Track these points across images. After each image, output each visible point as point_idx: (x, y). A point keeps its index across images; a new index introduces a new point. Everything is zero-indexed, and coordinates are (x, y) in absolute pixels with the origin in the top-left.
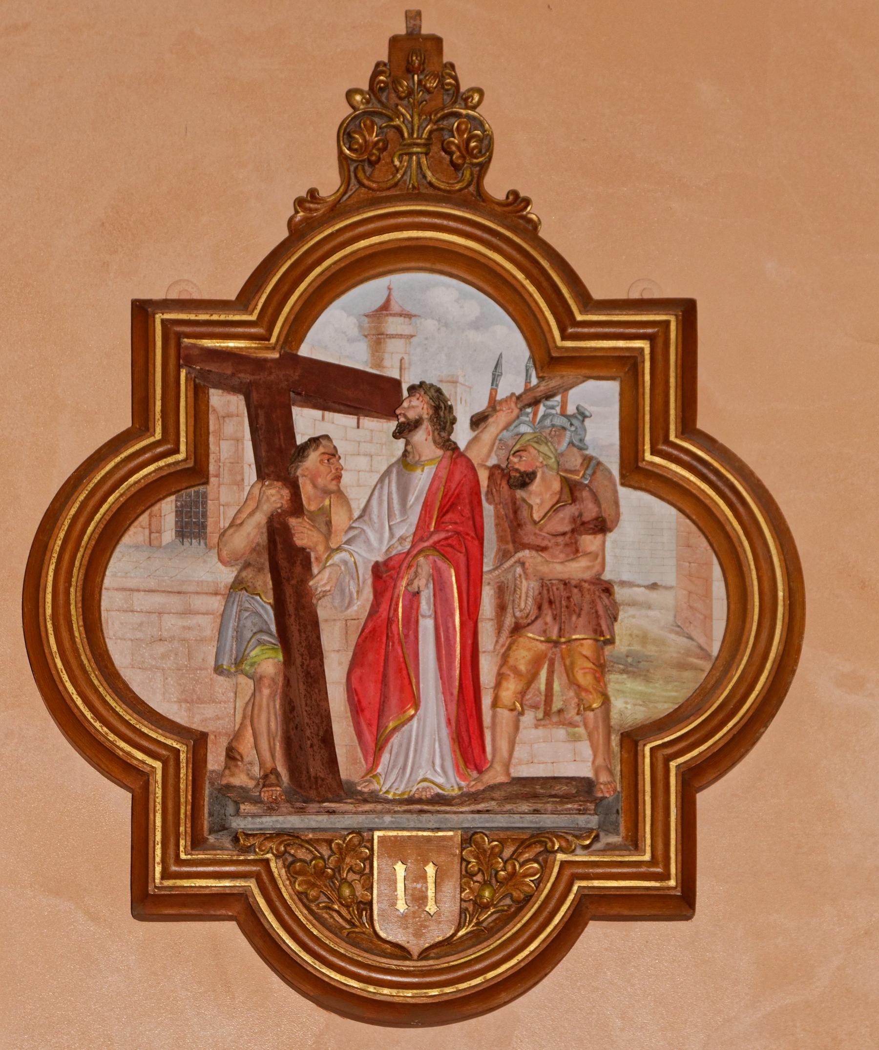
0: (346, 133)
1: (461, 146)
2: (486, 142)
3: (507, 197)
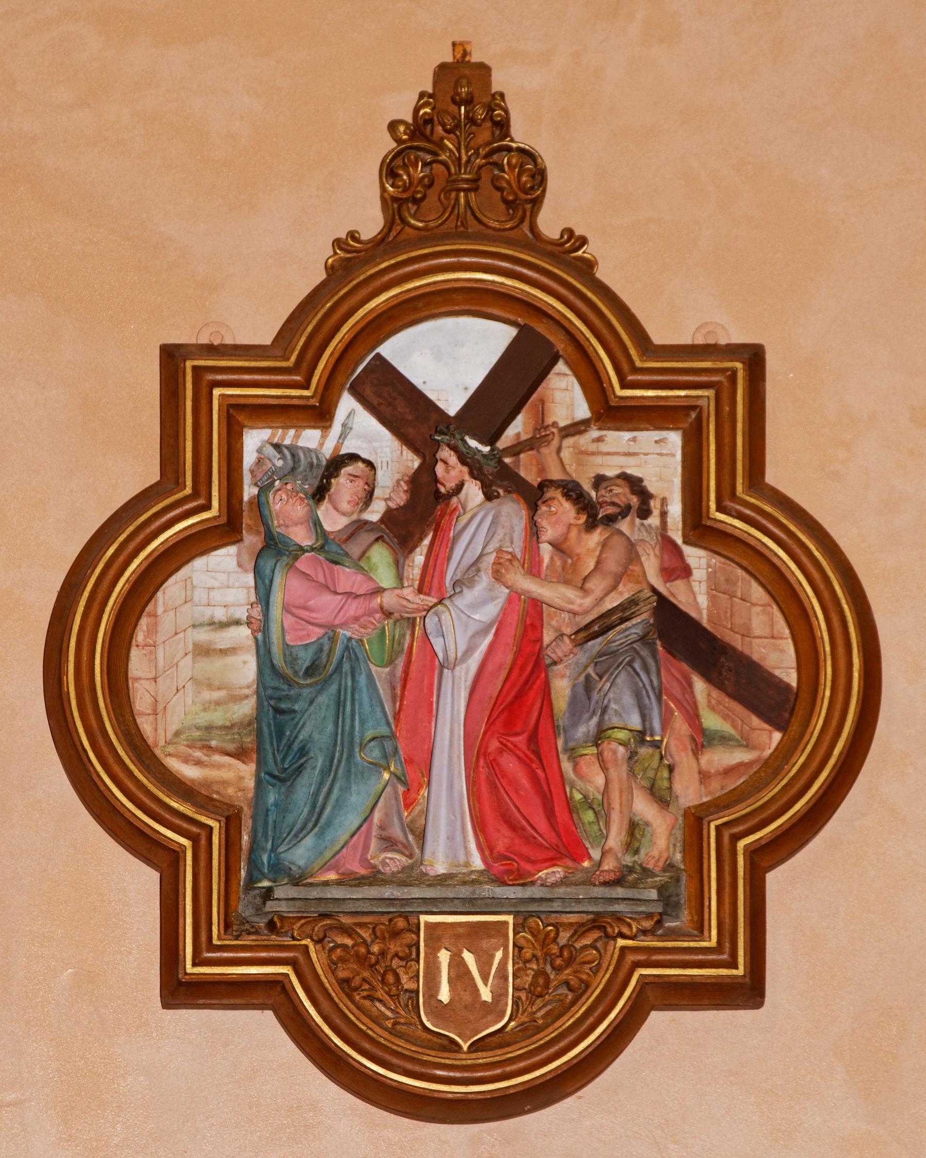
0: (389, 170)
1: (512, 182)
2: (538, 178)
3: (562, 237)
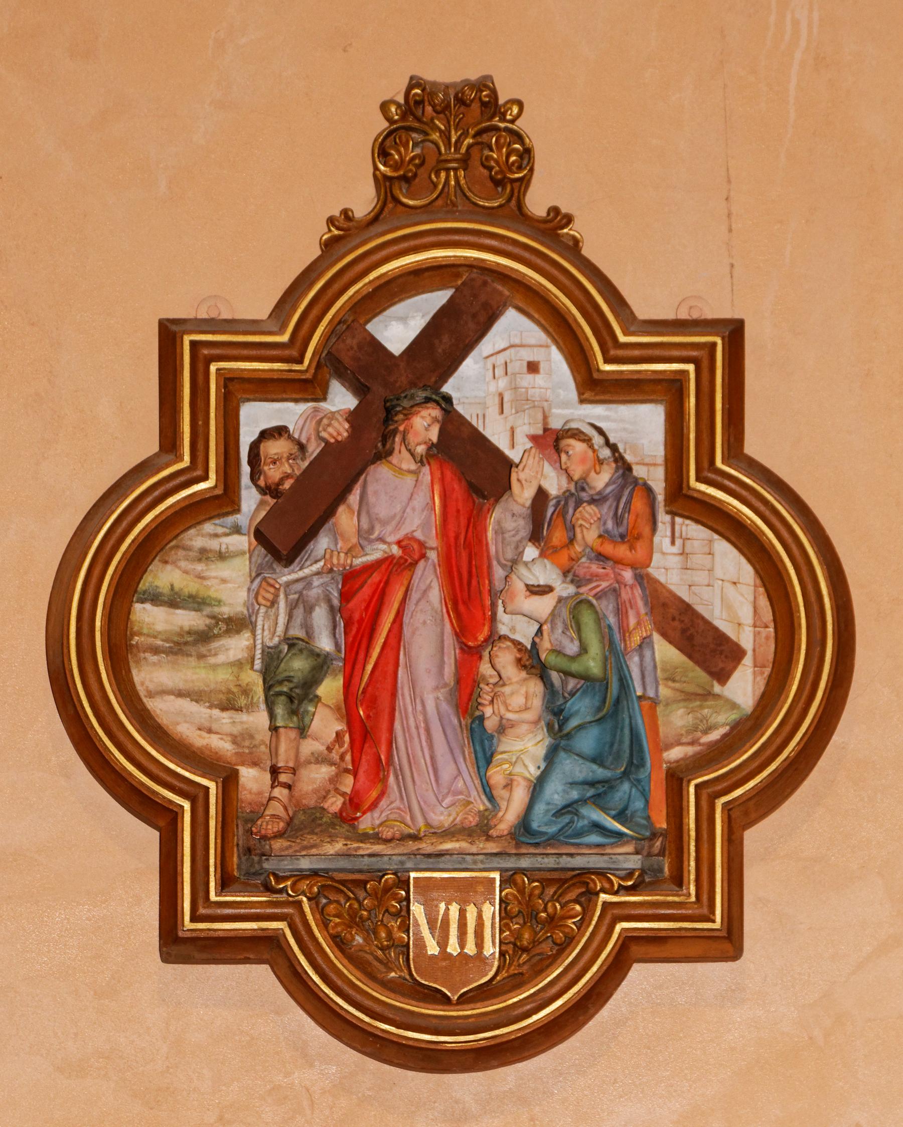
0: (382, 151)
2: (526, 156)
3: (548, 214)
